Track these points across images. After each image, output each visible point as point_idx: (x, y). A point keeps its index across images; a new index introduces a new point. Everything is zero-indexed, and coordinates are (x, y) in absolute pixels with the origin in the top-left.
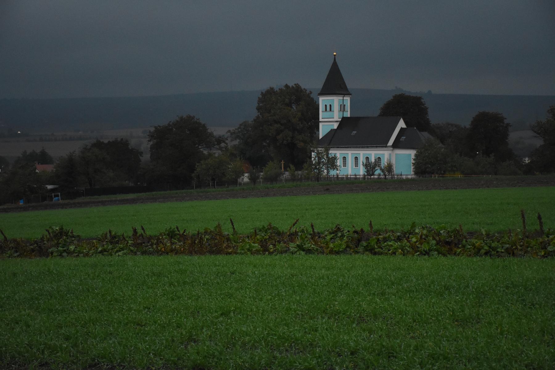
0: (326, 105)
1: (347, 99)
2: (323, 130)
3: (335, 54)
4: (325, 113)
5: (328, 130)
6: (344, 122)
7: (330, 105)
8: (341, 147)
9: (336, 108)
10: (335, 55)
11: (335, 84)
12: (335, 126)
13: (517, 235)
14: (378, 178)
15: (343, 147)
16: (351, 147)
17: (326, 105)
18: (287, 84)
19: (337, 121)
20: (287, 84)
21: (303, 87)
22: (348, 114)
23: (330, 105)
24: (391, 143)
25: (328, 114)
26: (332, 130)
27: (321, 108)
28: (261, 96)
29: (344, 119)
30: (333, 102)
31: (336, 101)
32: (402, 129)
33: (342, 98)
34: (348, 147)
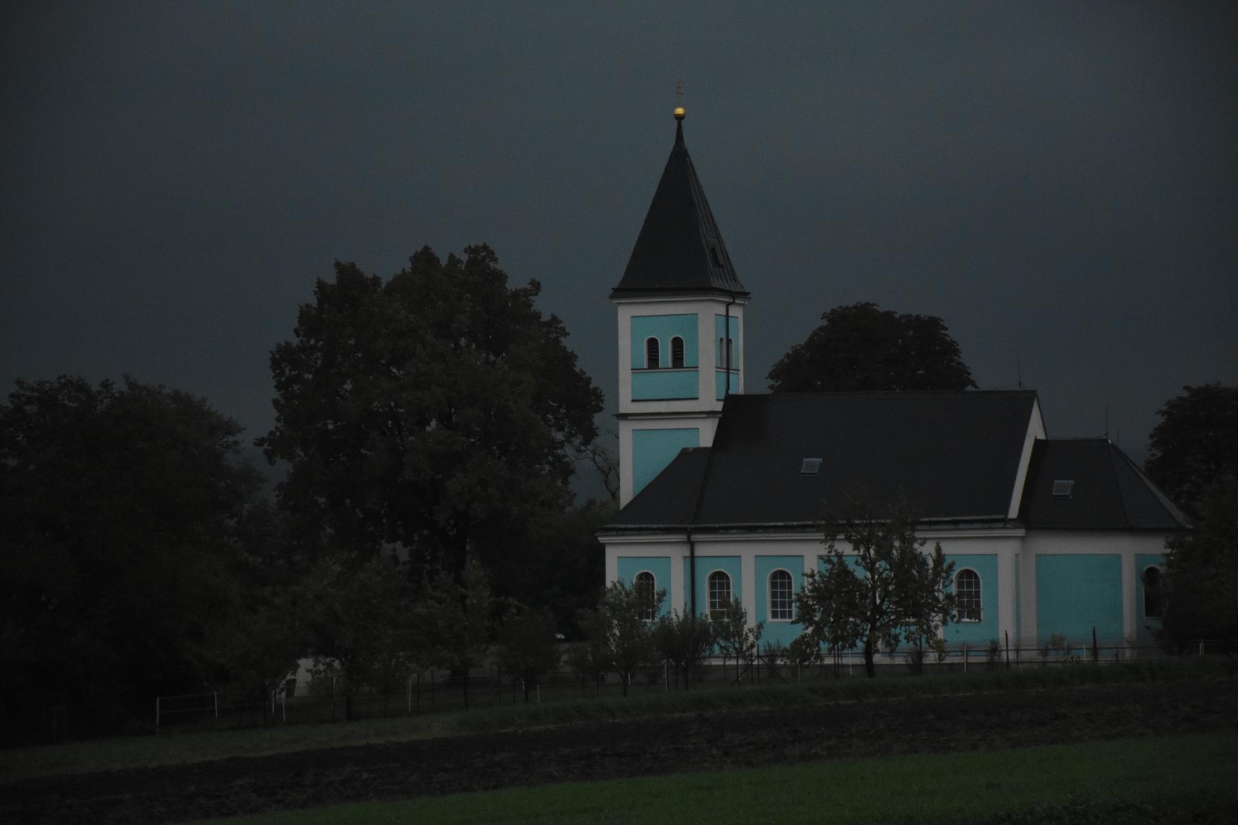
0: (653, 344)
2: (636, 458)
3: (680, 111)
4: (654, 377)
5: (666, 455)
6: (736, 414)
7: (677, 344)
8: (766, 529)
9: (705, 353)
10: (680, 118)
11: (677, 250)
14: (991, 665)
16: (726, 530)
17: (653, 344)
18: (426, 249)
19: (710, 414)
20: (426, 249)
21: (368, 273)
22: (738, 387)
23: (677, 344)
24: (1013, 513)
26: (684, 453)
27: (628, 351)
28: (314, 302)
31: (704, 321)
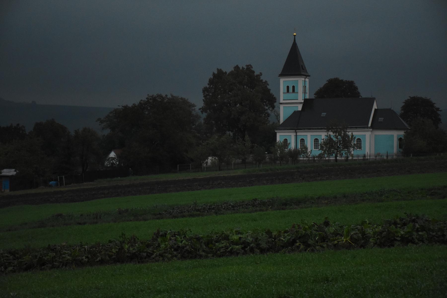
0: (288, 87)
1: (307, 80)
3: (295, 34)
4: (288, 95)
7: (294, 87)
8: (313, 129)
10: (295, 36)
11: (294, 65)
12: (300, 107)
13: (232, 236)
14: (364, 160)
15: (315, 129)
17: (288, 87)
19: (301, 103)
20: (237, 66)
22: (307, 97)
23: (294, 87)
24: (370, 125)
25: (291, 95)
28: (212, 77)
29: (305, 100)
30: (298, 84)
31: (300, 82)
32: (375, 109)
33: (304, 79)
34: (310, 129)
